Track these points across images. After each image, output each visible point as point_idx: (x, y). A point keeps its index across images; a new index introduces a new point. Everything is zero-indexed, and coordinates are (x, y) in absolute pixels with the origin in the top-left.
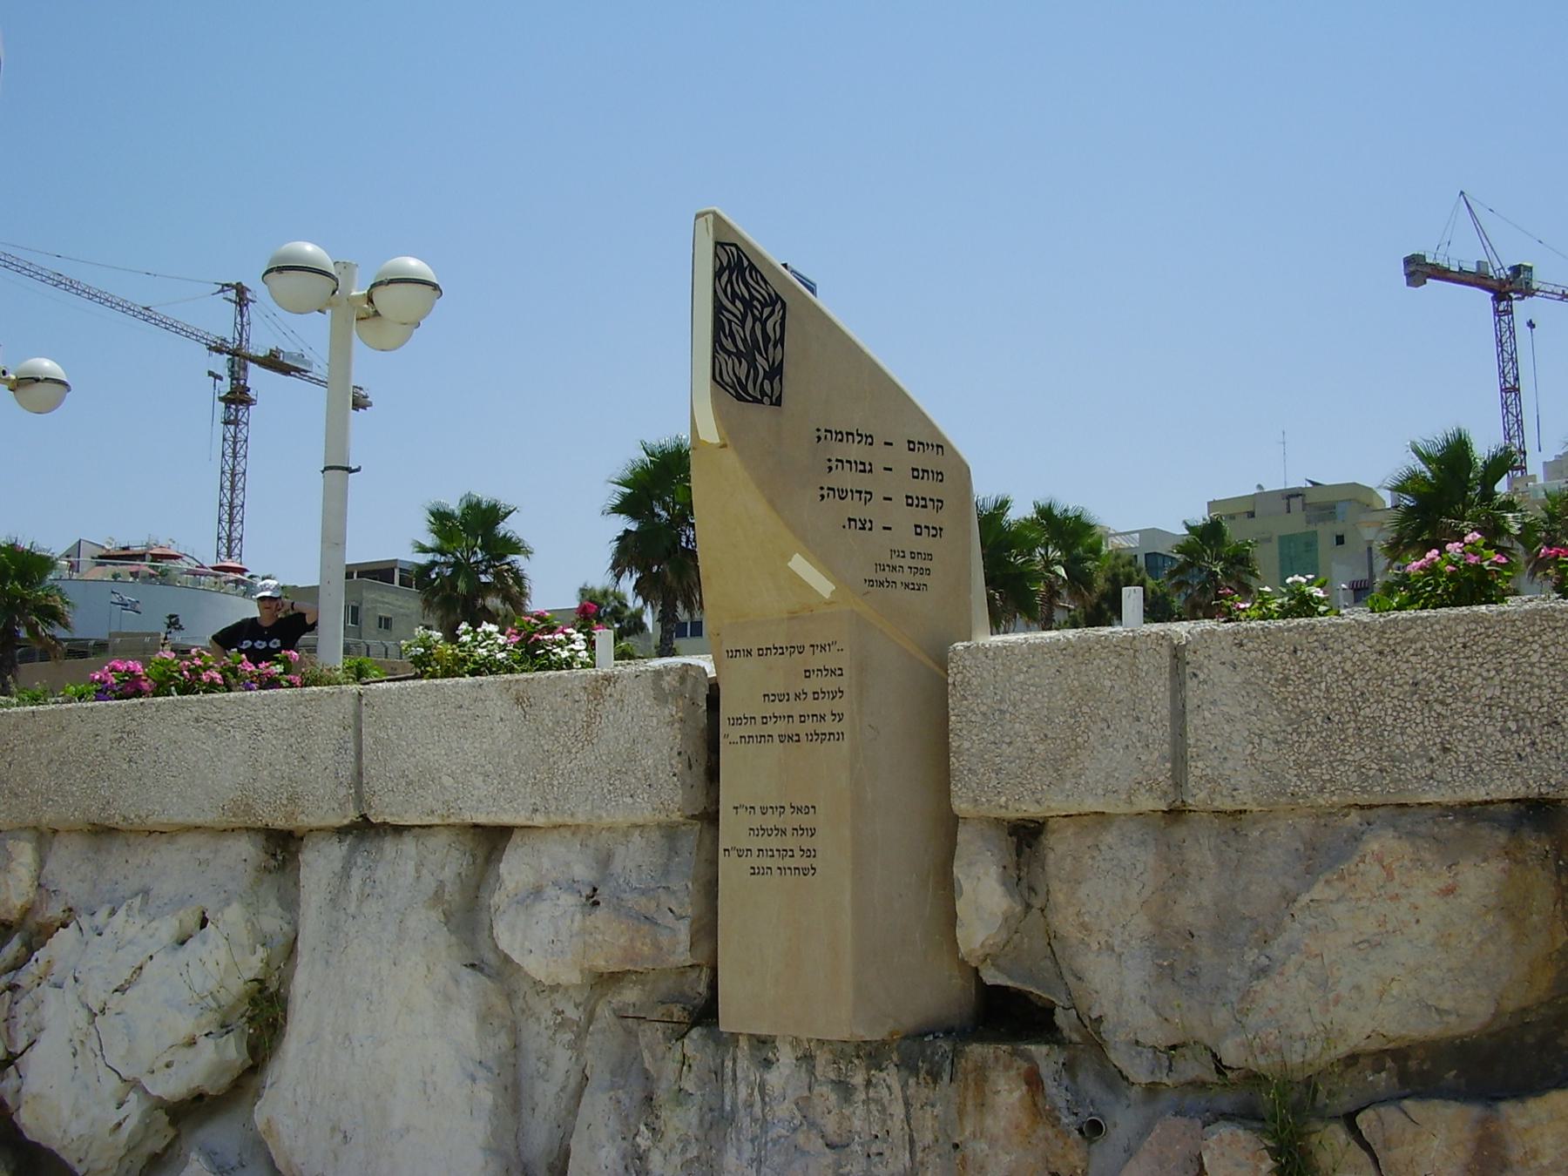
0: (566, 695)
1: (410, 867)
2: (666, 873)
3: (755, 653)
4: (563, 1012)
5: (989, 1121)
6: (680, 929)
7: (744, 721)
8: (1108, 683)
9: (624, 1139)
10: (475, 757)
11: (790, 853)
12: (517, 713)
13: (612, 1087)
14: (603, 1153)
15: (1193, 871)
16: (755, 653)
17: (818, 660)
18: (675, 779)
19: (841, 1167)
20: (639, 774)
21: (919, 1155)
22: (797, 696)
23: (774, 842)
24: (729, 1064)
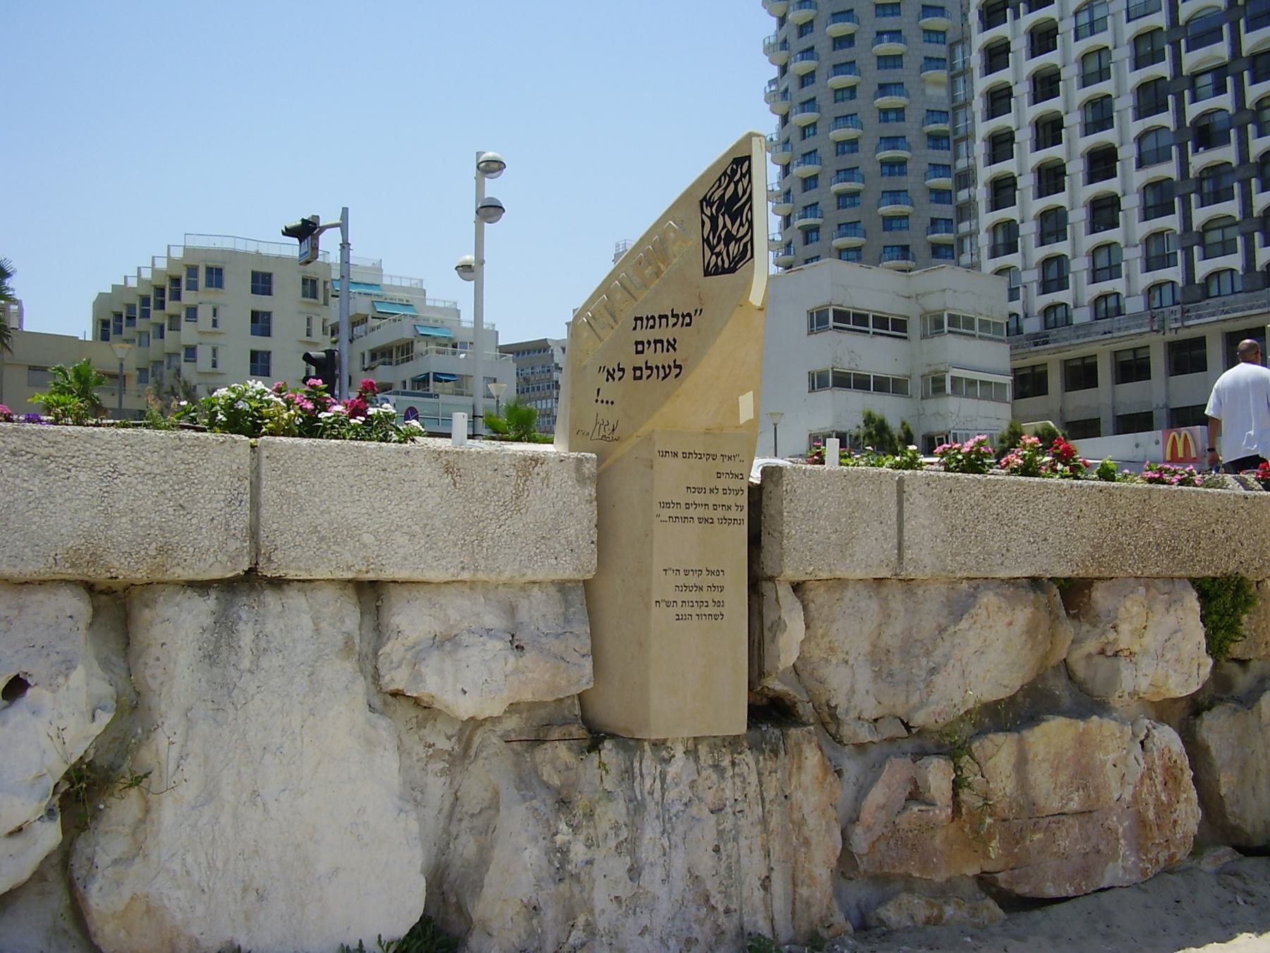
0: (496, 470)
1: (306, 620)
2: (567, 621)
3: (680, 455)
4: (434, 745)
5: (803, 777)
6: (585, 665)
7: (672, 505)
8: (868, 500)
9: (544, 838)
10: (400, 518)
11: (705, 604)
12: (447, 481)
13: (524, 799)
14: (527, 854)
15: (893, 614)
16: (680, 455)
17: (726, 467)
18: (593, 546)
19: (720, 825)
20: (563, 541)
21: (768, 806)
22: (711, 491)
23: (694, 596)
24: (636, 764)
